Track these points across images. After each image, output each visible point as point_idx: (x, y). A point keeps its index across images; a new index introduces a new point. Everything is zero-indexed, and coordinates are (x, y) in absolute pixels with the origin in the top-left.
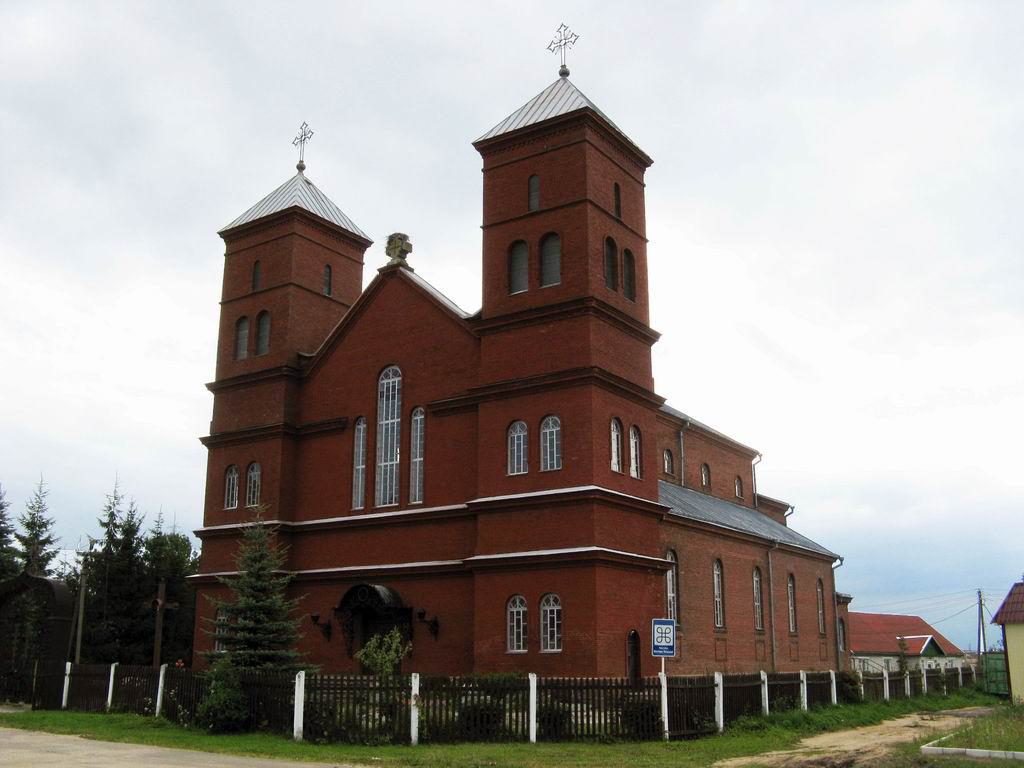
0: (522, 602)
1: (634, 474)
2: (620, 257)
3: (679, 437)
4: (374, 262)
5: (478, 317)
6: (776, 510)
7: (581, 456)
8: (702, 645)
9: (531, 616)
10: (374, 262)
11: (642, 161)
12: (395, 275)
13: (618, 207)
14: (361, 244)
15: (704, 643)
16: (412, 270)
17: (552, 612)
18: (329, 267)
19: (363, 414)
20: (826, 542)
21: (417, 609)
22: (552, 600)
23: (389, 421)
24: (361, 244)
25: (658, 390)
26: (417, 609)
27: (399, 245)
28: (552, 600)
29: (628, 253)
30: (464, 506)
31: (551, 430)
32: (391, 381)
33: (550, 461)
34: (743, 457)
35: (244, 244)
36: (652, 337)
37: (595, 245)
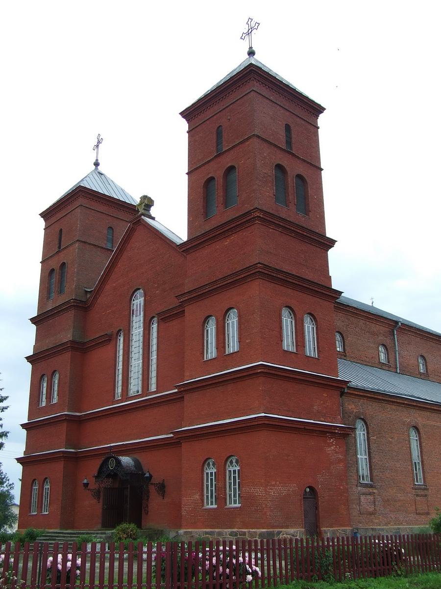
2: (291, 181)
3: (394, 335)
5: (190, 241)
8: (399, 500)
9: (221, 475)
11: (316, 109)
13: (289, 143)
15: (402, 498)
16: (153, 219)
19: (121, 328)
21: (156, 479)
22: (234, 461)
23: (137, 331)
25: (335, 286)
26: (156, 479)
28: (234, 461)
31: (233, 321)
32: (138, 301)
33: (233, 346)
35: (54, 219)
36: (331, 243)
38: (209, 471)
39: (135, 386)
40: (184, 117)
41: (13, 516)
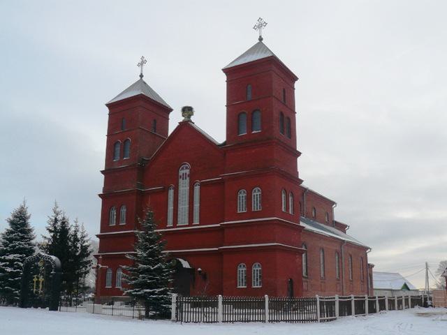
0: (244, 266)
1: (290, 213)
4: (174, 121)
5: (225, 143)
6: (342, 227)
7: (269, 204)
9: (249, 273)
10: (174, 121)
11: (294, 78)
12: (186, 126)
14: (168, 110)
17: (257, 270)
18: (155, 120)
20: (362, 241)
23: (184, 186)
24: (168, 110)
27: (187, 111)
29: (288, 118)
30: (219, 225)
31: (257, 193)
33: (256, 206)
34: (330, 204)
36: (299, 154)
37: (276, 115)
38: (241, 270)
39: (183, 220)
40: (224, 72)
41: (86, 289)
